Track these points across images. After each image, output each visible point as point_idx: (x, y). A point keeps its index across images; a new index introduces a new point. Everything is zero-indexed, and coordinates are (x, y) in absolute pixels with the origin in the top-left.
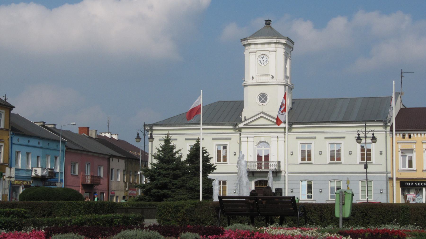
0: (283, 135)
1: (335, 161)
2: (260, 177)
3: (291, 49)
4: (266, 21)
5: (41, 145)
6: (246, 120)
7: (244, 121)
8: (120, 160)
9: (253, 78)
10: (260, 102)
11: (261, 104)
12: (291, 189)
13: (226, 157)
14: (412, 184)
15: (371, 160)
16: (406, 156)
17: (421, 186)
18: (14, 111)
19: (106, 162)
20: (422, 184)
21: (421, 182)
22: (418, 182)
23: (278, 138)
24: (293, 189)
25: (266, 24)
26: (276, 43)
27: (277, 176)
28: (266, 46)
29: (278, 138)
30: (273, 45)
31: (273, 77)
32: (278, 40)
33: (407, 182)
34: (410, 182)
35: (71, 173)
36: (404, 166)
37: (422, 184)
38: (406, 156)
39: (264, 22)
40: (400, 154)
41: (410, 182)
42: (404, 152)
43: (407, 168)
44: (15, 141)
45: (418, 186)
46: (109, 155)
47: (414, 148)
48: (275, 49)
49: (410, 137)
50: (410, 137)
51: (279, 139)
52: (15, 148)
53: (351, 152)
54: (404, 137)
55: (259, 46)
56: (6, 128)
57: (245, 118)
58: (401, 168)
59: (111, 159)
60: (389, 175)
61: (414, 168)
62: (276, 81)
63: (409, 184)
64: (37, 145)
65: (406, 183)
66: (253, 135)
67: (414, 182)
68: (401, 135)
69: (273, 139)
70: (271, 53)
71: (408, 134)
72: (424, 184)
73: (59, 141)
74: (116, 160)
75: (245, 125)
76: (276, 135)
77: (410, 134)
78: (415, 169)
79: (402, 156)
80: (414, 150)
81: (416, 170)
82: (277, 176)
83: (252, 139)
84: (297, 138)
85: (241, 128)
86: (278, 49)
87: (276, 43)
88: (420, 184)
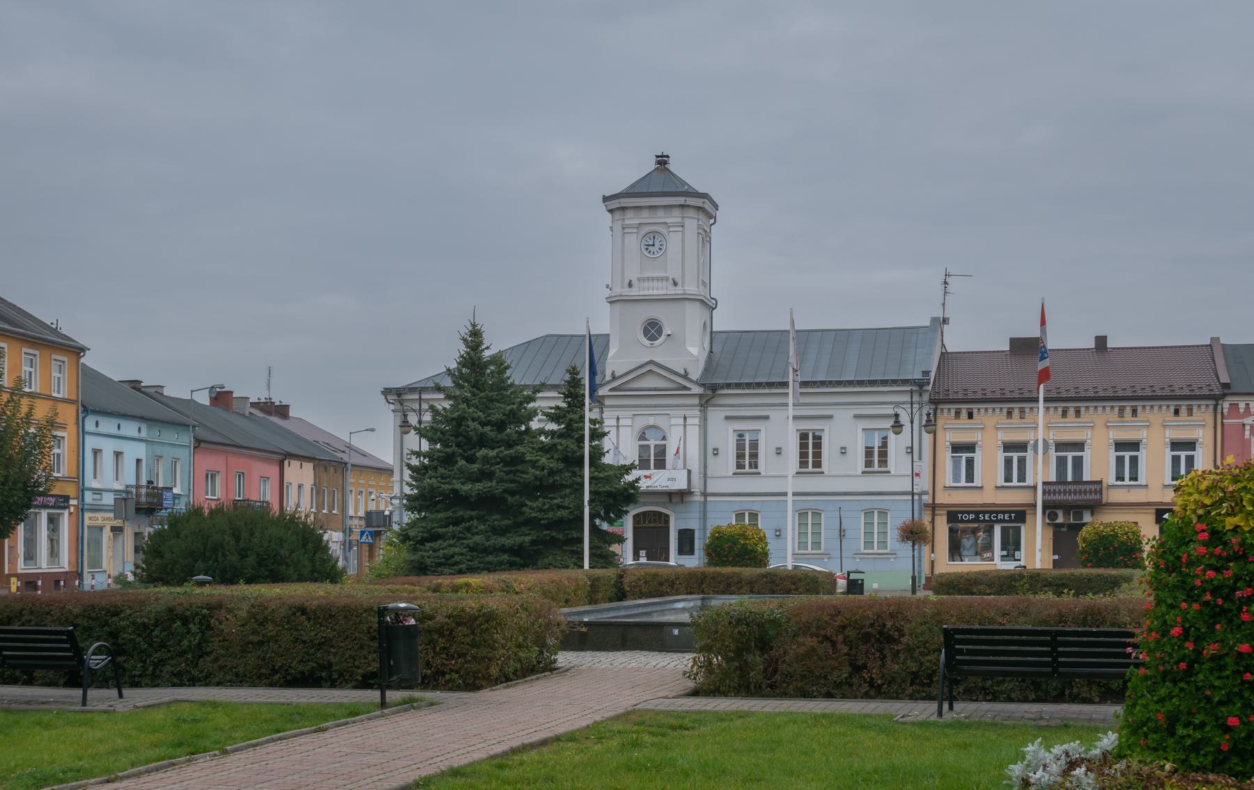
0: (696, 412)
1: (810, 469)
2: (652, 504)
3: (712, 221)
4: (657, 157)
5: (144, 434)
6: (614, 378)
7: (608, 382)
8: (304, 464)
9: (630, 285)
10: (645, 339)
11: (647, 343)
12: (776, 531)
13: (800, 462)
14: (972, 516)
15: (820, 467)
16: (961, 457)
17: (991, 521)
18: (86, 360)
19: (274, 470)
20: (994, 517)
21: (991, 513)
22: (984, 513)
23: (685, 418)
24: (779, 531)
25: (659, 163)
26: (683, 206)
27: (682, 502)
28: (660, 213)
29: (685, 418)
30: (676, 212)
31: (675, 284)
32: (687, 199)
33: (963, 513)
34: (969, 513)
35: (207, 494)
36: (956, 478)
37: (994, 517)
38: (961, 457)
39: (654, 160)
40: (949, 454)
41: (969, 513)
42: (957, 448)
43: (963, 483)
44: (90, 425)
45: (984, 521)
46: (281, 454)
47: (1201, 435)
48: (679, 220)
49: (970, 416)
50: (970, 416)
51: (689, 421)
52: (91, 443)
53: (845, 448)
54: (1064, 414)
55: (645, 213)
56: (70, 398)
57: (613, 373)
58: (949, 482)
59: (286, 462)
60: (925, 497)
61: (977, 482)
62: (682, 292)
63: (966, 517)
64: (135, 434)
65: (960, 515)
66: (630, 413)
67: (977, 513)
68: (1116, 410)
69: (674, 421)
70: (671, 229)
71: (1132, 406)
72: (997, 517)
73: (189, 426)
74: (295, 464)
75: (610, 390)
76: (682, 412)
77: (971, 409)
78: (980, 485)
79: (952, 457)
80: (1200, 440)
81: (981, 488)
82: (682, 502)
83: (629, 422)
84: (727, 418)
85: (603, 397)
86: (687, 221)
87: (683, 206)
88: (990, 517)
